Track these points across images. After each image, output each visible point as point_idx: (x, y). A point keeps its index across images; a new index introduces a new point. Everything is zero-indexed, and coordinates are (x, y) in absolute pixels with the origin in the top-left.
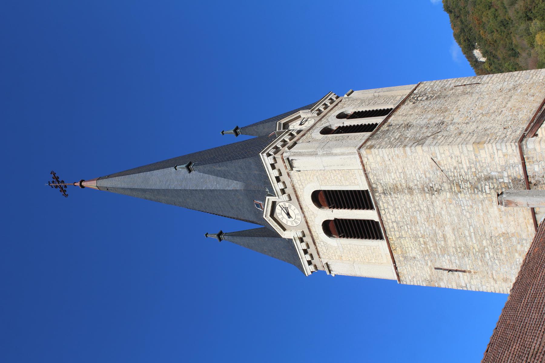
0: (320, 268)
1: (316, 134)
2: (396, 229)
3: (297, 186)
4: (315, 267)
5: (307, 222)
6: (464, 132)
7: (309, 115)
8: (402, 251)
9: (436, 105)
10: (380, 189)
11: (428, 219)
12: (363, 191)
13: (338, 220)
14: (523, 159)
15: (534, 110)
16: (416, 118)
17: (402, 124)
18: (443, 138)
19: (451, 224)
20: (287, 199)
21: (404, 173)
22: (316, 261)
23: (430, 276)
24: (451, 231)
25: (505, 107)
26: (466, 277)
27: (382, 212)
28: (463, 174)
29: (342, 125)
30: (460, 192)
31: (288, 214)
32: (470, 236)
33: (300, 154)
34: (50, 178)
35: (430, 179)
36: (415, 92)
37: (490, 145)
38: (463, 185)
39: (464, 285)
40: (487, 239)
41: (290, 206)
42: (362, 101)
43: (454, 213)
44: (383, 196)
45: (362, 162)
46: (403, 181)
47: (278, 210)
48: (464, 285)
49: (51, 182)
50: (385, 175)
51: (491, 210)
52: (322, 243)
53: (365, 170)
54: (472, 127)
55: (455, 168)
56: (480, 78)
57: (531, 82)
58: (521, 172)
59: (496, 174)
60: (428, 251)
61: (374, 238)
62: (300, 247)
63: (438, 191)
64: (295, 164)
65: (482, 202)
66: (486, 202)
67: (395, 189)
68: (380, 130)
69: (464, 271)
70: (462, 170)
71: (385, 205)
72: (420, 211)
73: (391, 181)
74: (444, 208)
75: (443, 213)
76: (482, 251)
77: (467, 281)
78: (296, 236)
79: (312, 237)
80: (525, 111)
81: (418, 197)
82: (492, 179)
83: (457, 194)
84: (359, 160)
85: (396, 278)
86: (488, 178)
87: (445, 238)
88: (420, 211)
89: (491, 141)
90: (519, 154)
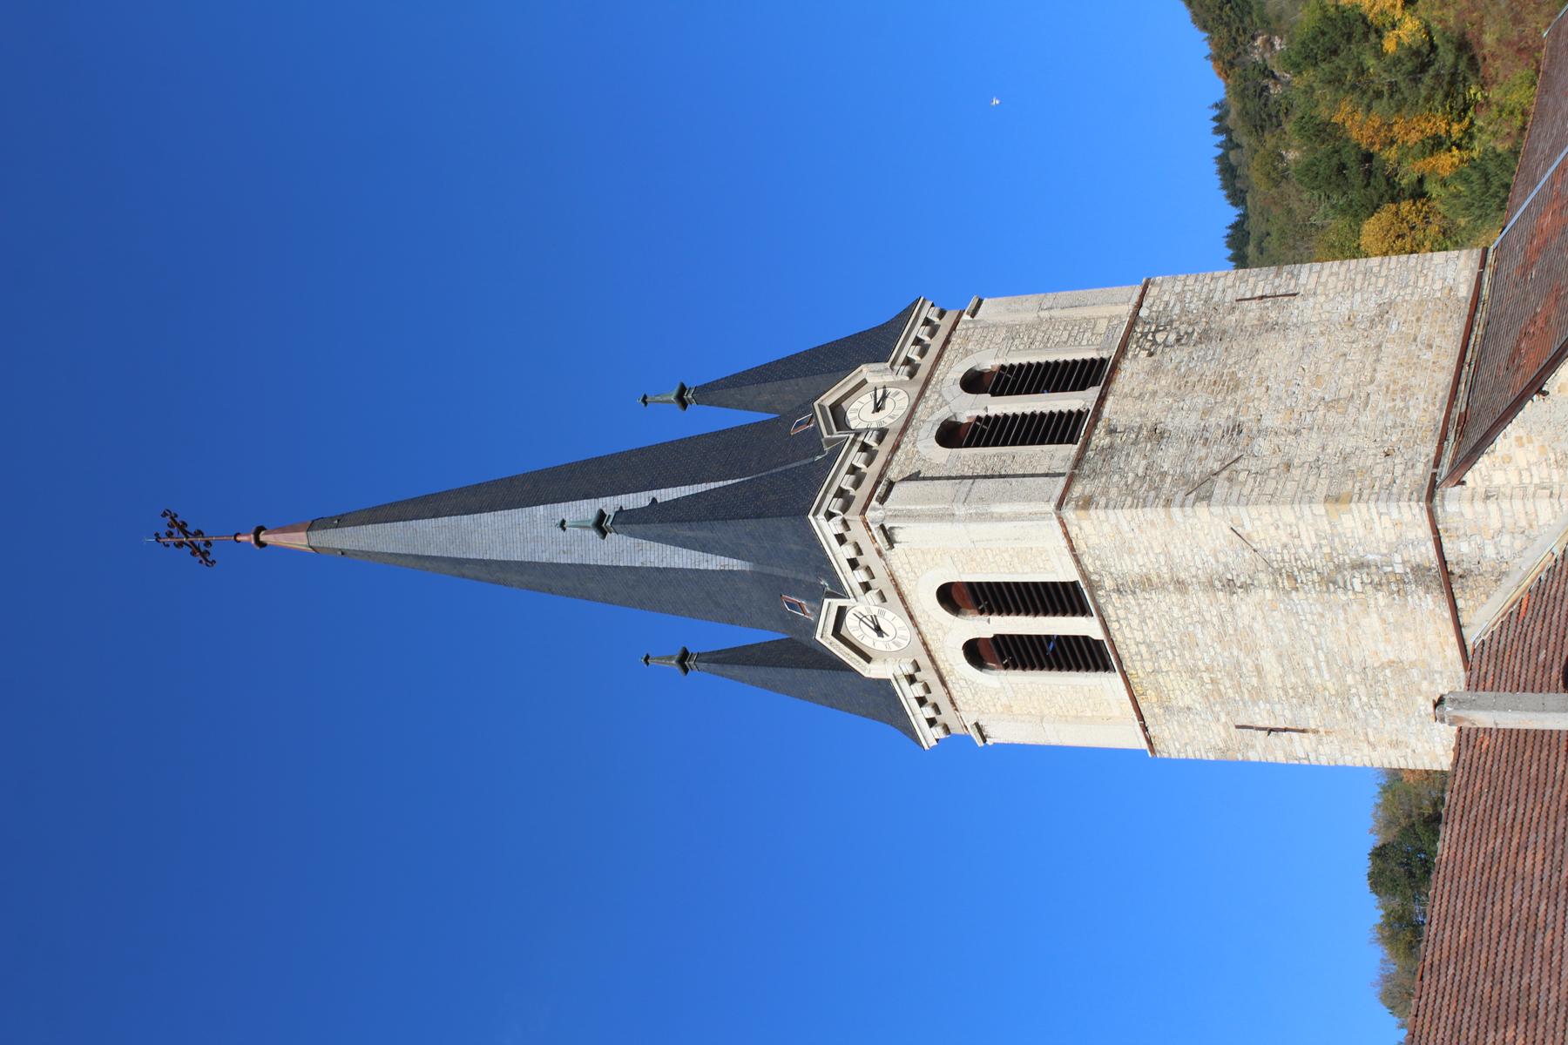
0: (956, 729)
1: (925, 449)
2: (1146, 655)
3: (901, 575)
4: (946, 729)
5: (925, 644)
6: (1296, 462)
7: (889, 378)
8: (1159, 697)
9: (1205, 362)
10: (1109, 583)
11: (1221, 637)
12: (1064, 584)
13: (1002, 636)
14: (1436, 531)
15: (1440, 394)
16: (1170, 408)
17: (1140, 428)
18: (1251, 481)
19: (1275, 646)
20: (877, 600)
21: (1168, 555)
22: (947, 715)
23: (1225, 741)
24: (1274, 660)
25: (1372, 382)
26: (1306, 741)
27: (1113, 626)
28: (1304, 556)
29: (983, 414)
30: (1297, 589)
31: (878, 630)
32: (1318, 668)
33: (911, 516)
34: (162, 525)
35: (1226, 565)
36: (1143, 313)
37: (1363, 506)
38: (1302, 577)
39: (1302, 755)
40: (1355, 673)
41: (883, 614)
42: (1013, 332)
43: (1281, 626)
44: (1115, 596)
45: (1066, 534)
46: (1165, 569)
47: (850, 621)
48: (1302, 755)
49: (162, 534)
50: (1120, 557)
51: (1365, 622)
52: (962, 683)
53: (1072, 549)
54: (1308, 448)
55: (1285, 546)
56: (1291, 273)
57: (1416, 297)
58: (1433, 553)
59: (1378, 558)
60: (1221, 695)
61: (1088, 669)
62: (908, 694)
63: (1245, 587)
64: (899, 535)
65: (1345, 607)
66: (1355, 606)
67: (1146, 584)
68: (1092, 446)
69: (1303, 731)
70: (1301, 551)
71: (1121, 613)
72: (1204, 623)
73: (1137, 569)
74: (1259, 618)
75: (1256, 626)
76: (1345, 695)
77: (1308, 748)
78: (899, 673)
79: (938, 671)
80: (1421, 398)
81: (1198, 598)
82: (1369, 567)
83: (1288, 593)
84: (1059, 531)
85: (1145, 746)
86: (1360, 566)
87: (1259, 673)
88: (1204, 623)
89: (1365, 497)
90: (1427, 522)
